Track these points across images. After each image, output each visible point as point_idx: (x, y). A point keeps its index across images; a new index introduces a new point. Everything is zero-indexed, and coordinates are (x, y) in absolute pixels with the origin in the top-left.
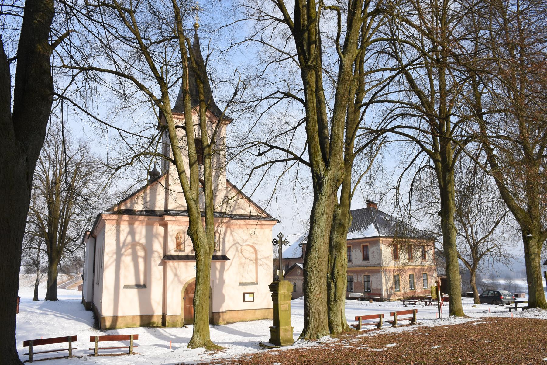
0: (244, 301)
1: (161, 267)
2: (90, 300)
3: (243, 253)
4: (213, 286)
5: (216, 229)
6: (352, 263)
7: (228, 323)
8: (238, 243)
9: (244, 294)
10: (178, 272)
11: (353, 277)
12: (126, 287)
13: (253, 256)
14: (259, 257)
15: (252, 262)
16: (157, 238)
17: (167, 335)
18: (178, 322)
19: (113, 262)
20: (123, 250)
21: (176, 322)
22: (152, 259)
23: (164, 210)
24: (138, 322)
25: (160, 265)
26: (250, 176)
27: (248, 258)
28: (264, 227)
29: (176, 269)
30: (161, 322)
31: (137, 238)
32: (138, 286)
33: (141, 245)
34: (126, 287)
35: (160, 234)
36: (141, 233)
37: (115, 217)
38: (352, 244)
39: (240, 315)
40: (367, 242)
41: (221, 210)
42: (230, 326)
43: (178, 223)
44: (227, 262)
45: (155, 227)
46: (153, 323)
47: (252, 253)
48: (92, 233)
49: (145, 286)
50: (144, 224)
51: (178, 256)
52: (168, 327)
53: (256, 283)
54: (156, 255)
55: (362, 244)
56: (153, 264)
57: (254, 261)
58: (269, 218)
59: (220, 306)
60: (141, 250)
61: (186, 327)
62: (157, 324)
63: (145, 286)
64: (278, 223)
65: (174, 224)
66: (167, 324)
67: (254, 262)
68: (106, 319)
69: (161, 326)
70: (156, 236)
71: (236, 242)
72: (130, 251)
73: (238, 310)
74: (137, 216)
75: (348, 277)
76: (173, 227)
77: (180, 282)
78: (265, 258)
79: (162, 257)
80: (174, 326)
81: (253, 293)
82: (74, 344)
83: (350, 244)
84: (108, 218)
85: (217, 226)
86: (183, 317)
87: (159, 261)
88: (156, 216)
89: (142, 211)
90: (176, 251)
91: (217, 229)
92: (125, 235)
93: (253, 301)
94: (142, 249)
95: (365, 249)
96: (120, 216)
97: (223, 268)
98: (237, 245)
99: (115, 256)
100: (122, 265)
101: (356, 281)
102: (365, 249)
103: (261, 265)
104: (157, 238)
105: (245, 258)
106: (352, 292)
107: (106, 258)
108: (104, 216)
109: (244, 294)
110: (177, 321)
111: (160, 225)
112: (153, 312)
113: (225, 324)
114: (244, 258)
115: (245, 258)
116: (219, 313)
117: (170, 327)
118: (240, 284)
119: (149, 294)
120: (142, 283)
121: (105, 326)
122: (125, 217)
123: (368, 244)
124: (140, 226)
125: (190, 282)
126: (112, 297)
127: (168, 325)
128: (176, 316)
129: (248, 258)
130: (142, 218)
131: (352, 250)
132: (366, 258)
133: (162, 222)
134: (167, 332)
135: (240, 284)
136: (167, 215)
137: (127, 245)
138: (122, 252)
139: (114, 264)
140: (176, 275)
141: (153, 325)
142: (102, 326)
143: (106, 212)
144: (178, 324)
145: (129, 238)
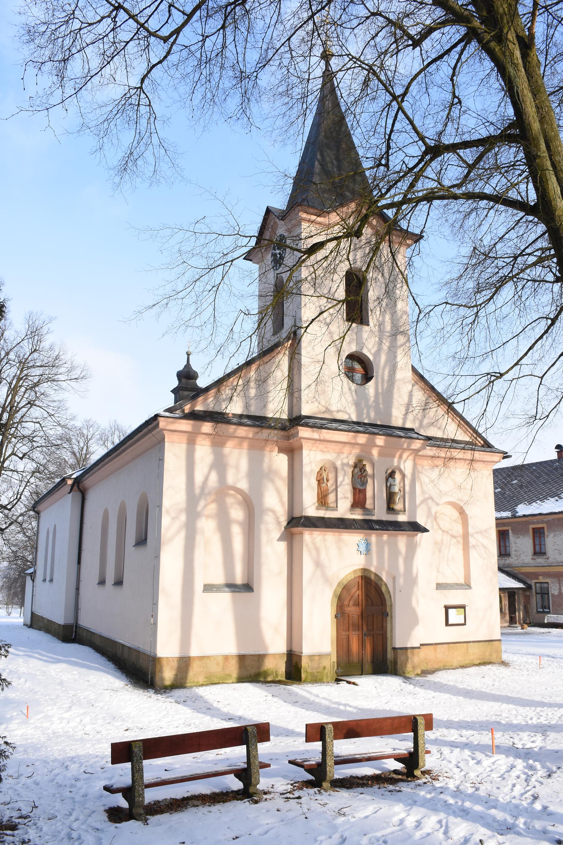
0: (447, 624)
1: (282, 546)
2: (71, 621)
3: (438, 520)
4: (394, 589)
5: (396, 464)
6: (548, 559)
7: (425, 673)
8: (431, 498)
9: (447, 608)
10: (323, 556)
11: (551, 585)
12: (208, 588)
13: (458, 529)
14: (471, 530)
15: (454, 541)
16: (273, 481)
17: (312, 698)
18: (326, 671)
19: (178, 532)
20: (202, 503)
21: (321, 669)
22: (263, 527)
23: (285, 416)
24: (233, 669)
25: (280, 539)
26: (554, 321)
27: (447, 532)
28: (476, 465)
29: (317, 550)
30: (283, 669)
31: (230, 479)
32: (232, 587)
33: (239, 491)
34: (208, 588)
35: (276, 473)
36: (237, 468)
37: (186, 425)
38: (547, 522)
39: (440, 654)
40: (542, 522)
41: (404, 422)
42: (430, 678)
43: (321, 446)
44: (420, 536)
45: (267, 453)
46: (266, 674)
47: (455, 521)
48: (77, 481)
49: (248, 587)
50: (245, 445)
51: (322, 519)
52: (306, 682)
53: (467, 585)
54: (269, 518)
55: (532, 526)
56: (264, 538)
57: (461, 540)
58: (487, 446)
59: (408, 634)
60: (238, 507)
61: (349, 682)
62: (277, 675)
63: (248, 587)
64: (504, 458)
65: (314, 448)
66: (303, 676)
67: (458, 542)
68: (164, 663)
69: (284, 679)
70: (271, 474)
71: (426, 496)
72: (212, 508)
73: (436, 644)
74: (233, 427)
75: (538, 585)
76: (312, 453)
77: (327, 580)
78: (481, 532)
79: (285, 524)
80: (316, 680)
81: (463, 607)
82: (263, 748)
83: (504, 525)
84: (172, 427)
85: (397, 456)
86: (334, 658)
87: (277, 533)
88: (270, 427)
89: (241, 416)
90: (318, 509)
91: (399, 462)
92: (206, 470)
93: (464, 624)
94: (239, 503)
95: (538, 534)
96: (198, 423)
97: (412, 549)
98: (430, 501)
99: (183, 518)
100: (199, 540)
101: (556, 593)
102: (538, 534)
103: (474, 547)
104: (273, 481)
105: (443, 531)
106: (549, 613)
107: (165, 521)
108: (162, 423)
109: (447, 608)
110: (324, 668)
111: (281, 450)
112: (266, 648)
113: (418, 675)
114: (440, 532)
115: (443, 531)
116: (406, 649)
117: (310, 682)
118: (440, 586)
119: (257, 606)
120: (239, 580)
121: (162, 679)
122: (207, 427)
123: (544, 525)
124: (236, 451)
125: (349, 578)
126: (176, 614)
127: (306, 678)
128: (320, 656)
129: (447, 532)
130: (242, 431)
131: (546, 533)
132: (539, 552)
133: (285, 443)
134: (311, 693)
135: (440, 586)
136: (302, 425)
137: (209, 493)
138: (199, 508)
139: (183, 534)
140: (318, 564)
141: (265, 678)
142: (157, 679)
143: (167, 414)
144: (327, 676)
145: (214, 477)
